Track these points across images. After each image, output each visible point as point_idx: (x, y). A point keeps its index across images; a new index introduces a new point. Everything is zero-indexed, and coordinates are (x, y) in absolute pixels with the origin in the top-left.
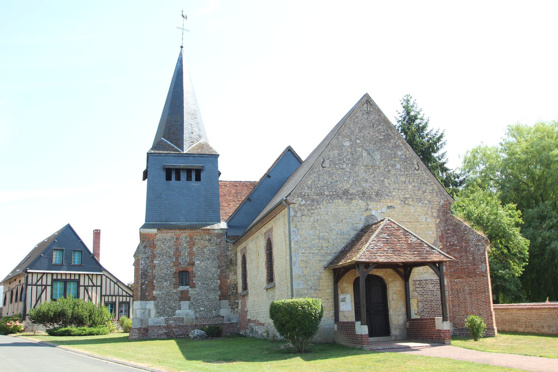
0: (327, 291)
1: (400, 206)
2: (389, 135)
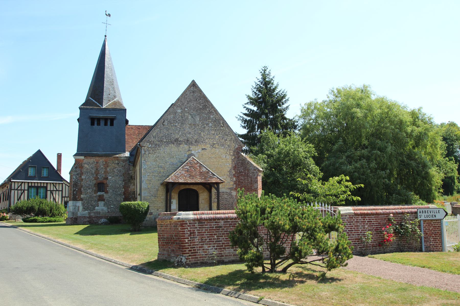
0: (162, 197)
1: (210, 149)
2: (206, 106)
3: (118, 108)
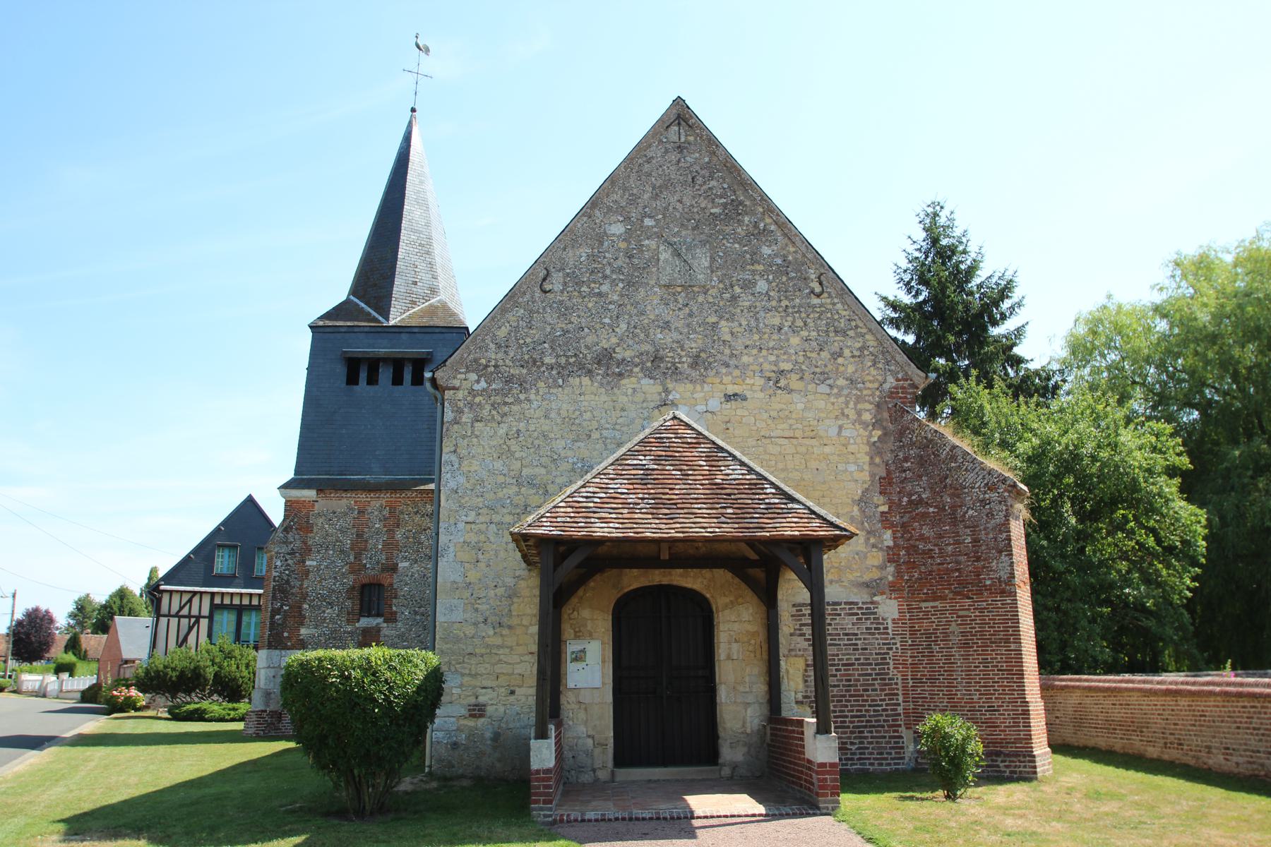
1: (761, 395)
3: (442, 324)
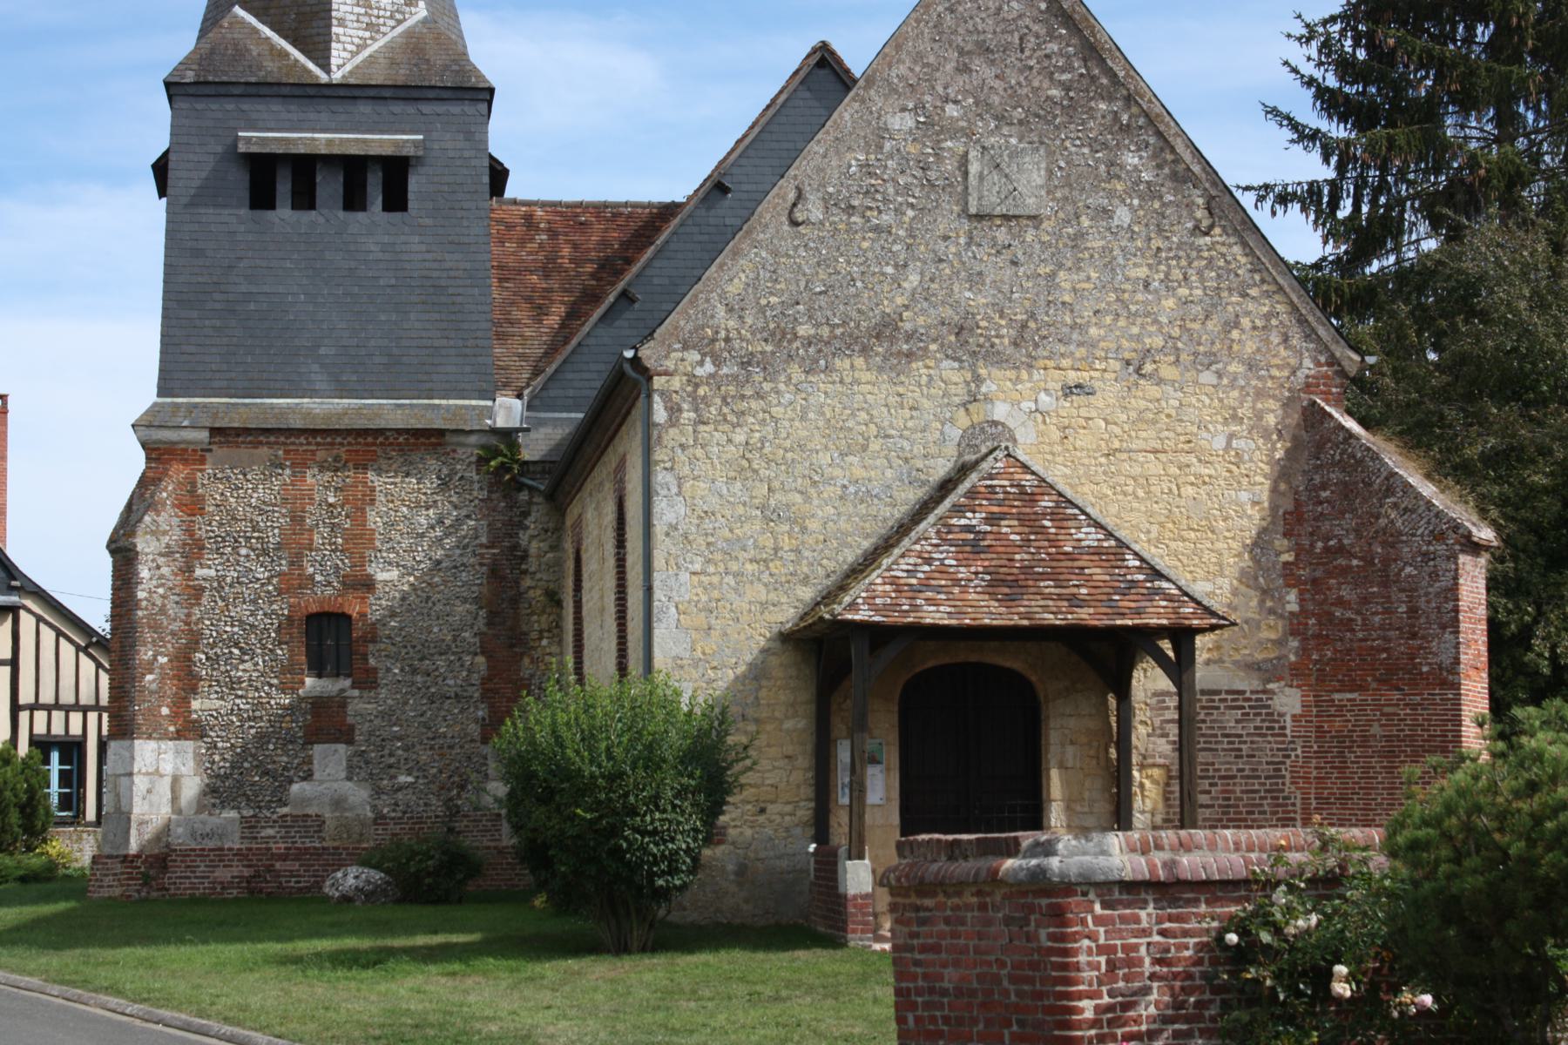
0: (788, 725)
